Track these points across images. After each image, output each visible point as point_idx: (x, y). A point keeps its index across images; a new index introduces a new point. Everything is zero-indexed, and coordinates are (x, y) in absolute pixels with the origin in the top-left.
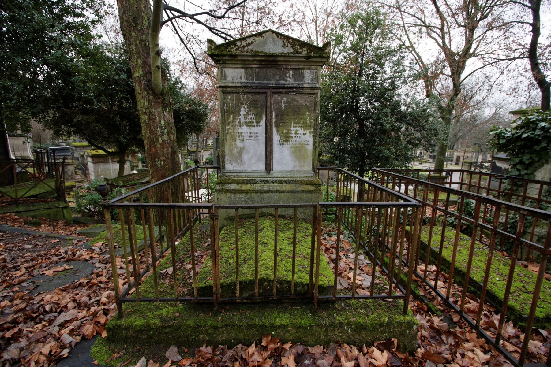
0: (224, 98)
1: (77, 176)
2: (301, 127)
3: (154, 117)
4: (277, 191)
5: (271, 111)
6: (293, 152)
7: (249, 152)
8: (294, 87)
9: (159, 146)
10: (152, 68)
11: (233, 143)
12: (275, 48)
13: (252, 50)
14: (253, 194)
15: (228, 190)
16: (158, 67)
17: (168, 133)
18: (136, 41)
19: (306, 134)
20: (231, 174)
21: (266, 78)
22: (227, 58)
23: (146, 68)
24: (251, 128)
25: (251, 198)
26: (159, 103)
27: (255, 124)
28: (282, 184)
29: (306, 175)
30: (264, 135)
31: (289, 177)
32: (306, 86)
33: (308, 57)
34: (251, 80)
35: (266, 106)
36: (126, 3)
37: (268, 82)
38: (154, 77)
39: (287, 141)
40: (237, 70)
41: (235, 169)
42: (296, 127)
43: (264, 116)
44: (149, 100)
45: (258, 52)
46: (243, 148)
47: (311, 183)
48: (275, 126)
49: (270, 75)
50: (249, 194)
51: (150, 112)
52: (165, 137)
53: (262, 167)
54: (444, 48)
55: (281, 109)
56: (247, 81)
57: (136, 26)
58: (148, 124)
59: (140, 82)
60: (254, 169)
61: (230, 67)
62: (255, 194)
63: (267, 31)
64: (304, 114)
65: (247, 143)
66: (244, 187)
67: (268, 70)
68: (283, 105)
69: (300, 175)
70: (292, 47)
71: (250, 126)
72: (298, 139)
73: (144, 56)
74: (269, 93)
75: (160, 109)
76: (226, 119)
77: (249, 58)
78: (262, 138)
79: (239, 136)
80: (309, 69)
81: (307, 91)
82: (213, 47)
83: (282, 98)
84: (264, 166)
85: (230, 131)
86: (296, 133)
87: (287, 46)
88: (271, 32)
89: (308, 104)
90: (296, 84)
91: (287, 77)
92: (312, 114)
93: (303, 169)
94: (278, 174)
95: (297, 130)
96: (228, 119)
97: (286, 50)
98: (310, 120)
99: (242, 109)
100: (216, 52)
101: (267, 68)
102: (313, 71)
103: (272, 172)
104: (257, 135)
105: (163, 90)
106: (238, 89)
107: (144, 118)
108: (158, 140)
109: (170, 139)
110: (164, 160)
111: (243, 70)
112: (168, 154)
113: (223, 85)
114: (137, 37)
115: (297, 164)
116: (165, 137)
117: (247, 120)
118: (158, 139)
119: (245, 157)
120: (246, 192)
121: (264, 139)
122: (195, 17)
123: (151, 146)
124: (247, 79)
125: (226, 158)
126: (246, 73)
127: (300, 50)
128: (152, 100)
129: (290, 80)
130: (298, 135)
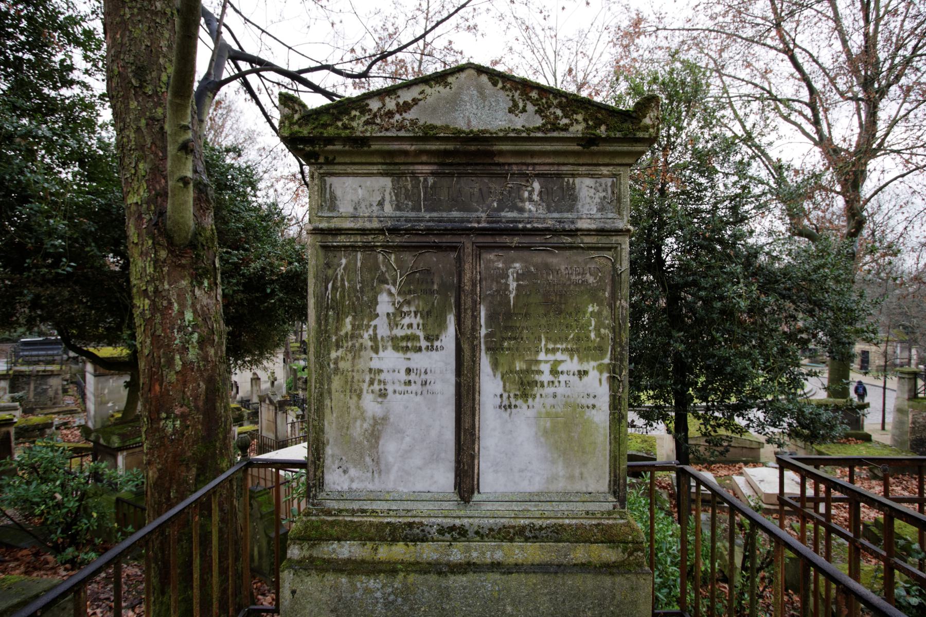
0: (328, 265)
1: (67, 398)
2: (571, 352)
3: (165, 303)
4: (495, 566)
5: (475, 302)
6: (546, 432)
7: (400, 431)
8: (547, 230)
9: (173, 377)
10: (170, 183)
11: (352, 403)
12: (490, 115)
13: (414, 122)
14: (412, 578)
15: (329, 561)
16: (185, 181)
17: (202, 343)
18: (138, 119)
19: (586, 373)
20: (342, 505)
21: (457, 203)
22: (338, 147)
23: (159, 182)
24: (409, 355)
25: (406, 592)
26: (183, 267)
27: (424, 343)
28: (511, 540)
29: (592, 507)
30: (452, 378)
31: (535, 515)
32: (583, 224)
33: (589, 141)
34: (413, 209)
35: (459, 289)
36: (122, 37)
37: (465, 215)
38: (173, 204)
39: (525, 396)
40: (369, 182)
41: (355, 486)
42: (554, 351)
43: (451, 320)
44: (156, 261)
45: (433, 127)
46: (385, 419)
47: (609, 537)
48: (488, 349)
49: (472, 194)
50: (401, 575)
51: (156, 291)
52: (192, 355)
53: (443, 479)
54: (824, 142)
55: (507, 296)
56: (398, 213)
57: (141, 87)
58: (148, 322)
59: (140, 217)
60: (419, 487)
61: (348, 175)
62: (420, 578)
63: (460, 69)
64: (579, 311)
65: (396, 403)
66: (385, 552)
67: (463, 180)
68: (513, 285)
69: (571, 506)
70: (539, 112)
71: (406, 349)
72: (561, 390)
73: (156, 155)
74: (469, 248)
75: (184, 283)
76: (331, 327)
77: (407, 147)
78: (446, 386)
79: (372, 383)
80: (592, 176)
81: (587, 240)
82: (296, 117)
83: (509, 263)
84: (451, 476)
85: (342, 365)
86: (554, 372)
87: (524, 110)
88: (472, 72)
89: (591, 280)
90: (550, 219)
91: (523, 201)
92: (606, 312)
93: (580, 486)
94: (496, 506)
95: (557, 363)
96: (338, 329)
97: (519, 122)
98: (597, 329)
99: (383, 298)
100: (305, 131)
101: (460, 175)
102: (603, 180)
103: (476, 497)
104: (429, 377)
105: (197, 234)
106: (370, 238)
107: (142, 304)
108: (170, 362)
109: (205, 358)
110: (183, 417)
111: (387, 182)
112: (196, 398)
113: (324, 225)
114: (142, 112)
115: (560, 469)
116: (192, 355)
117: (399, 332)
118: (173, 358)
119: (390, 447)
120: (391, 569)
121: (452, 390)
122: (304, 75)
123: (151, 379)
124: (398, 208)
125: (329, 451)
126: (397, 191)
127: (565, 121)
128: (164, 261)
129: (532, 207)
130: (562, 378)
